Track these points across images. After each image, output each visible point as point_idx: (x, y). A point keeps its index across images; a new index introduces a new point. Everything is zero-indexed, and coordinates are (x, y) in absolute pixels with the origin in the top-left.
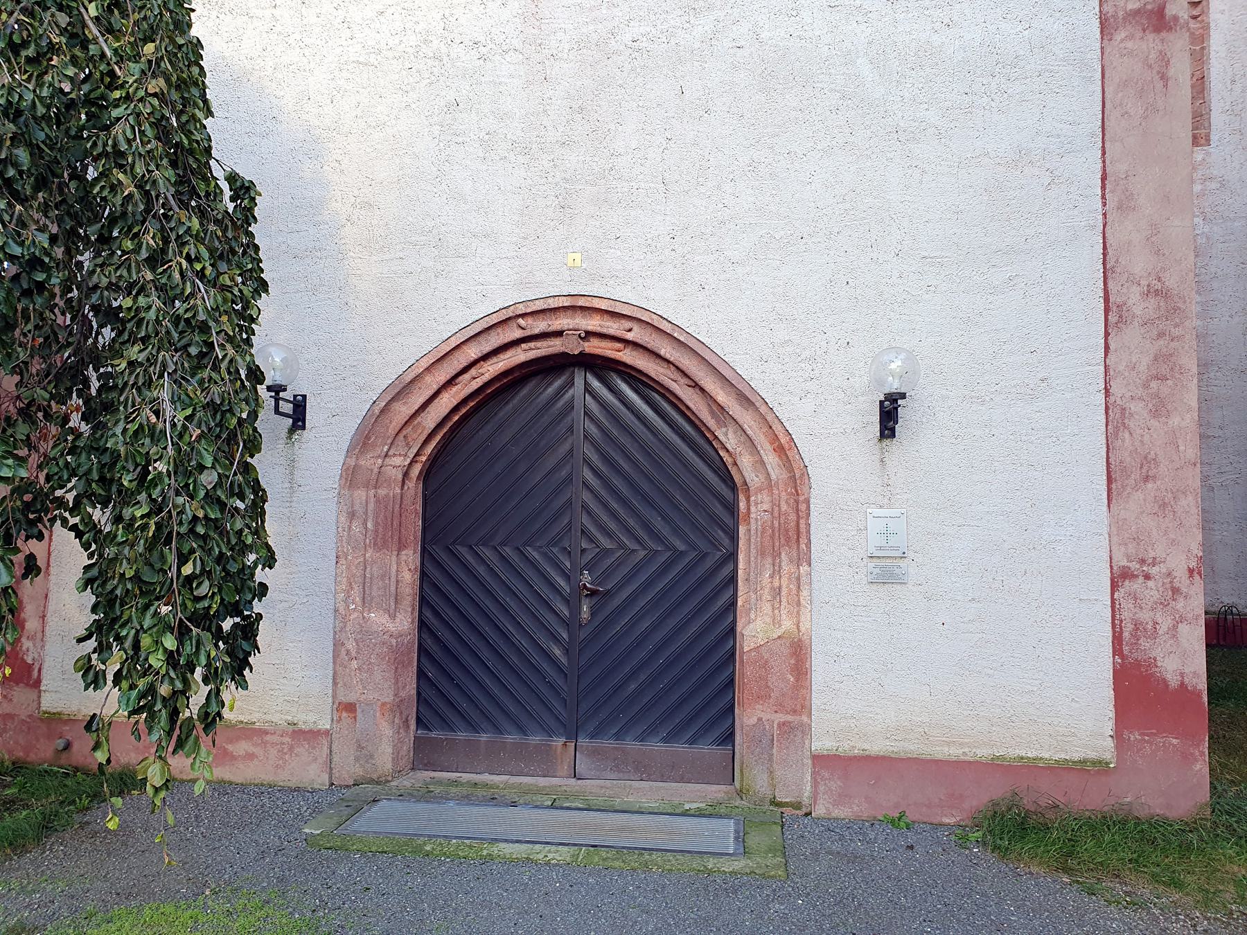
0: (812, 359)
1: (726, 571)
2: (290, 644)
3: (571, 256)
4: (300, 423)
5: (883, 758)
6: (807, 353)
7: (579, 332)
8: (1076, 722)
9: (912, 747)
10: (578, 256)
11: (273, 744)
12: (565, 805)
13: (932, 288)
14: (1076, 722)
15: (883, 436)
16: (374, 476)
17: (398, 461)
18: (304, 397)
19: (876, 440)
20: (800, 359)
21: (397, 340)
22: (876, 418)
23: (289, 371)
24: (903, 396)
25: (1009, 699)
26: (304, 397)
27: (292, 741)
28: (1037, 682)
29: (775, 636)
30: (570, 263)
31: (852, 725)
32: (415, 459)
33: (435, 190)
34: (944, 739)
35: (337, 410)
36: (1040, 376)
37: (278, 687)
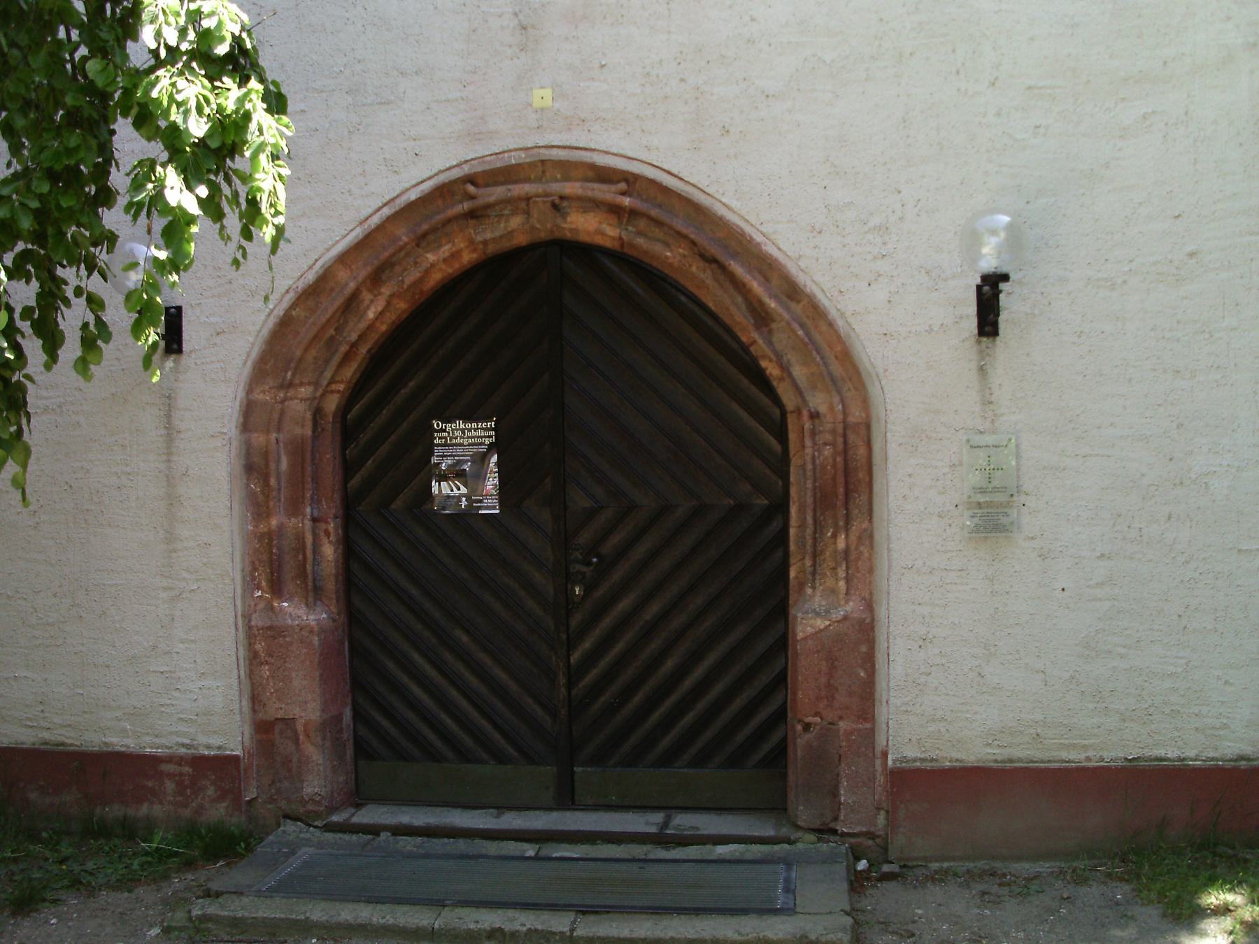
0: (883, 229)
1: (775, 525)
2: (181, 646)
3: (538, 93)
4: (175, 346)
5: (978, 768)
6: (875, 221)
7: (550, 199)
8: (1229, 710)
9: (1022, 751)
10: (547, 93)
11: (171, 776)
12: (554, 855)
13: (1041, 130)
14: (1229, 710)
15: (982, 333)
16: (276, 416)
17: (305, 391)
18: (179, 309)
19: (973, 340)
20: (866, 228)
21: (300, 224)
22: (972, 309)
23: (56, 214)
24: (1005, 278)
25: (1147, 684)
26: (179, 309)
27: (193, 771)
28: (1183, 661)
29: (839, 618)
30: (537, 103)
31: (943, 730)
32: (329, 389)
33: (347, 15)
34: (1062, 741)
35: (222, 326)
36: (1189, 249)
37: (169, 701)
